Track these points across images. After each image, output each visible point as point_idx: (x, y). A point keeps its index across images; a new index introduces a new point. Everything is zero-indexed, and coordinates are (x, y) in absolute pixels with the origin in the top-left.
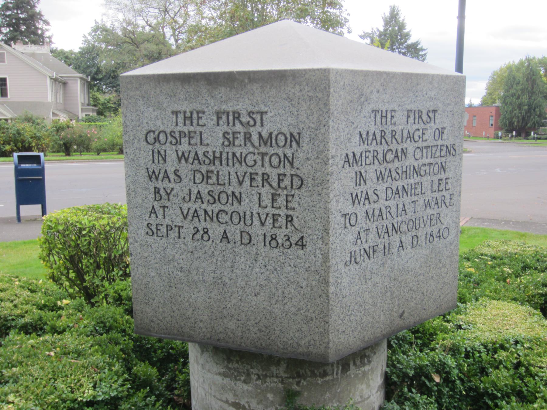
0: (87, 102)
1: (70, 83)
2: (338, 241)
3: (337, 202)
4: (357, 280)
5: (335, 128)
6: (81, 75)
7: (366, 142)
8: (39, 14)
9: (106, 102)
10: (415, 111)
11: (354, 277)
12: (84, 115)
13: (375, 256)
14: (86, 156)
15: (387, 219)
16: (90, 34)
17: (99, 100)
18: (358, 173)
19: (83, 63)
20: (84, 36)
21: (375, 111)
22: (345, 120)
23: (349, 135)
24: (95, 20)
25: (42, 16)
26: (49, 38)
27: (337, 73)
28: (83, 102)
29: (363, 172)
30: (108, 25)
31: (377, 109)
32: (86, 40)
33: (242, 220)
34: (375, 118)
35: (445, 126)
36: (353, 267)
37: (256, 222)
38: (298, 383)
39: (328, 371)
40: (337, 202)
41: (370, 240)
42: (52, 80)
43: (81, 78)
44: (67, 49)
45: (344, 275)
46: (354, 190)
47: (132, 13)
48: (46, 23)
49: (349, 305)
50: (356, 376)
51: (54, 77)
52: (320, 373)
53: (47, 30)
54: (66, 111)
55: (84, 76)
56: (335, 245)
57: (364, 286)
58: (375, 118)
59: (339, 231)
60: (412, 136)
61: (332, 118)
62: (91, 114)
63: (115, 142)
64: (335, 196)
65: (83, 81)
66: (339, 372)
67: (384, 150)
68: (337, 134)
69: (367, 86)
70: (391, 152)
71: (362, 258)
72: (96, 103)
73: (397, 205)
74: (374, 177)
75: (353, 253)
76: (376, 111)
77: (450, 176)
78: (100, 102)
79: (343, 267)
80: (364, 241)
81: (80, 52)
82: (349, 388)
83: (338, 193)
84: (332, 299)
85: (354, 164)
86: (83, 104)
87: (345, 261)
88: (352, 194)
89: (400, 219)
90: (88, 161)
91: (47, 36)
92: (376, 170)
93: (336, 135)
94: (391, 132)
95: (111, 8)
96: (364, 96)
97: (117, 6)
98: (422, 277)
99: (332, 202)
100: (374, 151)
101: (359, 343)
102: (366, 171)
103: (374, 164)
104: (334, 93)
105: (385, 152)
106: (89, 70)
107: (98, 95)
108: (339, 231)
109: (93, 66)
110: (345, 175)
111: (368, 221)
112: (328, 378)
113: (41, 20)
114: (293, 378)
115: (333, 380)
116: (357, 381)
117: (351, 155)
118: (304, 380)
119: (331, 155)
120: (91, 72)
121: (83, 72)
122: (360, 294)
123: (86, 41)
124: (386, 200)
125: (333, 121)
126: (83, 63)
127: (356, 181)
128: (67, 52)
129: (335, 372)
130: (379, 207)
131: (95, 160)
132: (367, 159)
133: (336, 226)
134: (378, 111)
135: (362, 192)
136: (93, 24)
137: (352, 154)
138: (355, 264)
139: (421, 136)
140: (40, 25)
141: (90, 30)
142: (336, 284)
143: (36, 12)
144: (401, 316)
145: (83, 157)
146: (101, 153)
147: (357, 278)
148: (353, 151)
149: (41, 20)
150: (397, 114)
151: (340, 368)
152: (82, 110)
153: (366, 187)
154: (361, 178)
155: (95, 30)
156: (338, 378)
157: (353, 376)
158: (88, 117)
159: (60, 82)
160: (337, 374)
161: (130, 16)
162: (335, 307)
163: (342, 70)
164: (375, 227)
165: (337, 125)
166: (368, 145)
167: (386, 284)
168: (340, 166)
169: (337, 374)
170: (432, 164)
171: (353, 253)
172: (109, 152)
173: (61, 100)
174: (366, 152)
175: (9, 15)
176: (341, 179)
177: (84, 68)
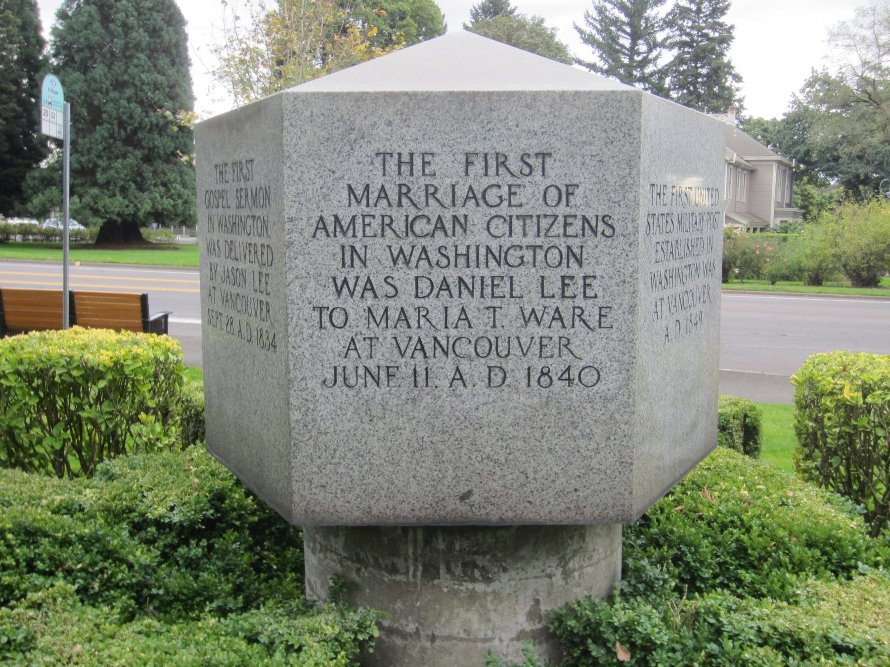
0: (787, 200)
1: (761, 170)
2: (307, 345)
3: (303, 287)
4: (349, 413)
5: (296, 178)
6: (779, 158)
7: (364, 201)
8: (729, 66)
9: (823, 201)
10: (486, 155)
11: (344, 406)
12: (778, 221)
13: (391, 384)
14: (755, 284)
15: (419, 327)
16: (802, 91)
17: (813, 198)
18: (347, 248)
19: (787, 138)
20: (794, 95)
21: (385, 155)
22: (316, 166)
23: (325, 190)
24: (813, 68)
25: (732, 68)
26: (740, 101)
27: (295, 99)
28: (779, 200)
29: (358, 247)
30: (833, 74)
31: (389, 151)
32: (796, 102)
33: (494, 348)
34: (384, 165)
35: (575, 182)
36: (340, 390)
37: (516, 351)
38: (358, 571)
39: (399, 566)
40: (303, 287)
41: (378, 356)
42: (731, 167)
43: (780, 163)
44: (767, 117)
45: (322, 400)
46: (338, 273)
47: (874, 49)
48: (738, 78)
49: (332, 447)
50: (454, 593)
51: (734, 162)
52: (386, 566)
53: (738, 90)
54: (749, 214)
55: (786, 160)
56: (301, 350)
57: (367, 427)
58: (384, 165)
59: (307, 332)
60: (479, 196)
61: (288, 164)
62: (790, 220)
63: (802, 265)
64: (297, 277)
65: (783, 168)
66: (419, 574)
67: (407, 216)
68: (300, 186)
69: (363, 115)
70: (425, 221)
71: (363, 381)
72: (806, 203)
73: (446, 308)
74: (384, 257)
75: (340, 370)
76: (384, 154)
77: (598, 274)
78: (814, 201)
79: (318, 386)
80: (364, 355)
81: (783, 121)
82: (437, 607)
83: (305, 275)
84: (297, 431)
85: (337, 233)
86: (778, 204)
87: (322, 379)
88: (334, 279)
89: (453, 333)
90: (755, 292)
91: (737, 98)
92: (390, 247)
93: (297, 189)
94: (424, 188)
95: (837, 45)
96: (356, 131)
97: (849, 41)
98: (520, 444)
99: (292, 285)
100: (383, 217)
101: (358, 514)
102: (366, 247)
103: (383, 235)
104: (290, 128)
105: (410, 220)
106: (796, 149)
107: (811, 189)
108: (307, 332)
109: (803, 142)
110: (320, 248)
111: (373, 325)
112: (398, 578)
113: (730, 74)
114: (353, 562)
115: (407, 584)
116: (455, 602)
117: (330, 221)
118: (366, 568)
119: (287, 216)
120: (798, 152)
121: (787, 152)
122: (358, 435)
123: (794, 102)
124: (417, 296)
125: (290, 167)
126: (787, 138)
127: (343, 259)
128: (767, 122)
129: (411, 573)
130: (399, 307)
131: (765, 292)
132: (367, 228)
133: (302, 322)
134: (391, 155)
135: (358, 278)
136: (808, 75)
137: (333, 219)
138: (345, 388)
139: (506, 196)
140: (729, 82)
141: (802, 84)
142: (303, 409)
143: (723, 64)
144: (464, 497)
145: (746, 286)
146: (777, 283)
147: (351, 409)
148: (334, 213)
149: (730, 74)
150: (437, 159)
151: (421, 568)
152: (777, 214)
153: (365, 271)
154: (355, 256)
155: (810, 84)
156: (415, 584)
157: (445, 590)
158: (784, 225)
159: (743, 169)
160: (414, 576)
161: (870, 56)
162: (302, 444)
163: (307, 94)
164: (389, 338)
165: (300, 174)
166: (368, 205)
167: (420, 434)
168: (306, 235)
169: (414, 576)
170: (541, 247)
171: (340, 370)
172: (794, 280)
173: (743, 197)
174: (364, 216)
175: (684, 71)
176: (309, 253)
177: (789, 146)
